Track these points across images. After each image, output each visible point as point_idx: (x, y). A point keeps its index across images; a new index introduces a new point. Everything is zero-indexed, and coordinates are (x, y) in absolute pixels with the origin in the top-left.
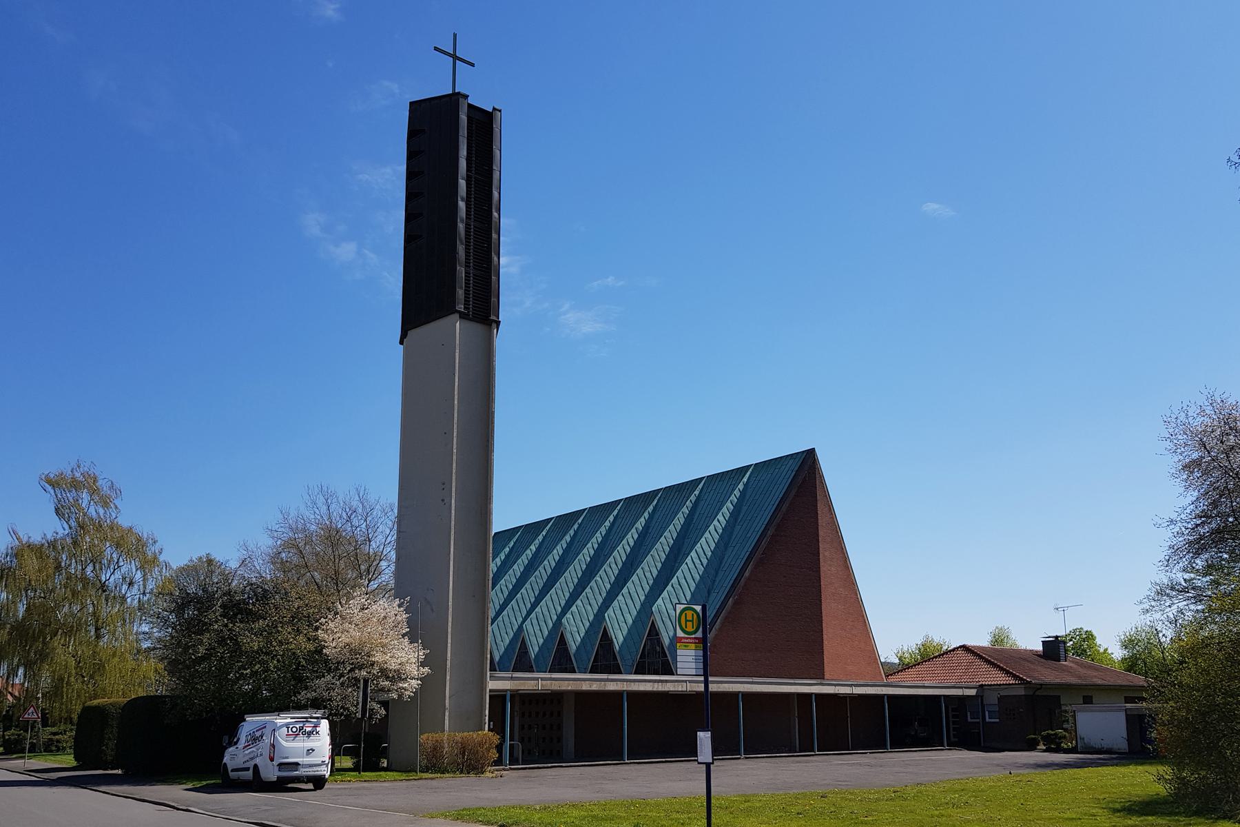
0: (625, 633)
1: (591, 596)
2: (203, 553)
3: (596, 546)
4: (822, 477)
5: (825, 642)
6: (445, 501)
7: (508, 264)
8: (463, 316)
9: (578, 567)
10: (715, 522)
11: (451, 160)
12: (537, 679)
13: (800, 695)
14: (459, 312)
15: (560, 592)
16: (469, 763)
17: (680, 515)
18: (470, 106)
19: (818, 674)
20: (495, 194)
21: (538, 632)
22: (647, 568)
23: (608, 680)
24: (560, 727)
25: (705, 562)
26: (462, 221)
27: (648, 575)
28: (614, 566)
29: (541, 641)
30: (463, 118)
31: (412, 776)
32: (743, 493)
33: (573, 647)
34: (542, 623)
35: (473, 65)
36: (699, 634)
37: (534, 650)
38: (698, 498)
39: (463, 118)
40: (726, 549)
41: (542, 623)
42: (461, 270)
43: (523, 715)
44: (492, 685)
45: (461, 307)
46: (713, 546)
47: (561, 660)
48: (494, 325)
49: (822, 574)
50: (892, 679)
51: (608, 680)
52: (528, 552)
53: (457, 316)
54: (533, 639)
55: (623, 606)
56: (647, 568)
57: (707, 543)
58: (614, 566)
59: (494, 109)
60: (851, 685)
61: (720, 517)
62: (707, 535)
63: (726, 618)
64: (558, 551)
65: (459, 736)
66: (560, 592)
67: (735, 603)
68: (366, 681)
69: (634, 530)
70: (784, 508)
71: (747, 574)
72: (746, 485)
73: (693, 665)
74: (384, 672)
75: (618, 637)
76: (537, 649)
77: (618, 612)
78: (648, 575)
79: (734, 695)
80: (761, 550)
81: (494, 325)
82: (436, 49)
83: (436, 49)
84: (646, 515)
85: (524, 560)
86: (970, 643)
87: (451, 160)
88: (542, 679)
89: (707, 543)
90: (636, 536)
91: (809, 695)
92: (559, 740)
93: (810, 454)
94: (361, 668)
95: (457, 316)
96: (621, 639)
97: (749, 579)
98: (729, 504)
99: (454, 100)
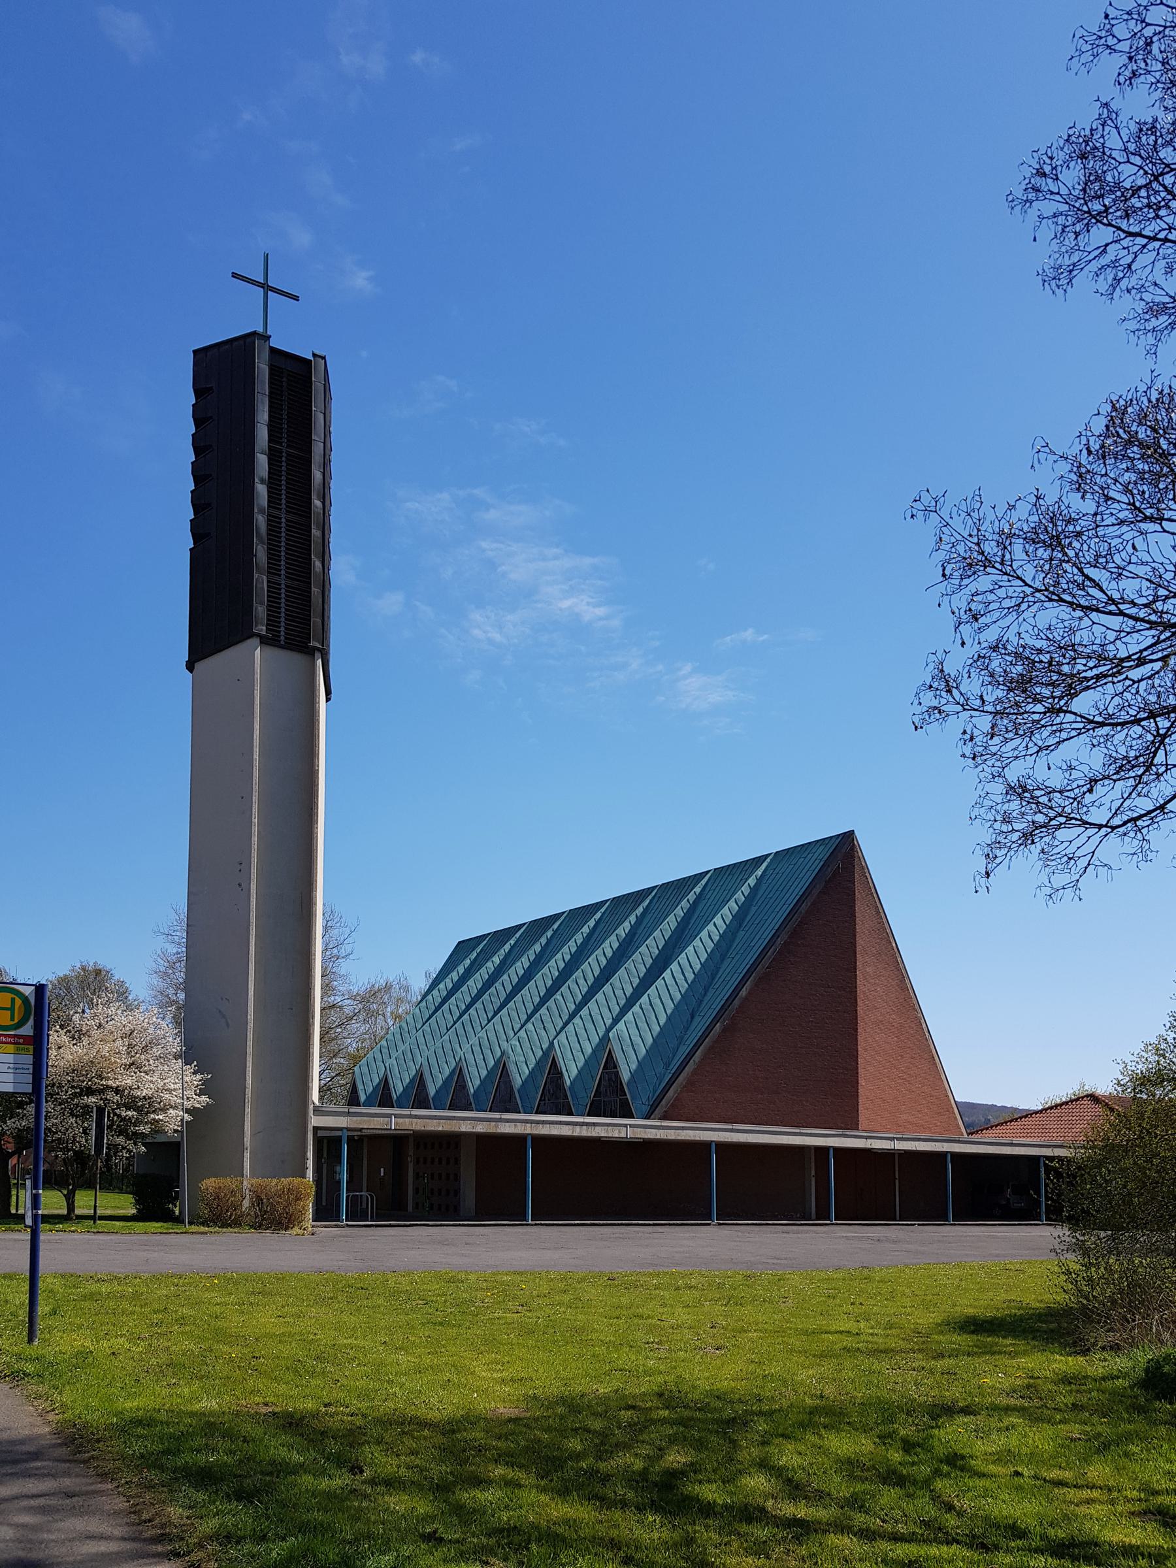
0: (581, 1064)
1: (546, 1018)
2: (109, 967)
3: (567, 957)
4: (865, 869)
5: (862, 1083)
6: (243, 887)
7: (345, 570)
8: (265, 641)
9: (541, 984)
10: (711, 927)
11: (258, 435)
12: (389, 1116)
13: (819, 1149)
14: (261, 637)
15: (513, 1014)
16: (272, 1217)
17: (671, 918)
18: (273, 351)
19: (848, 1121)
20: (317, 475)
21: (481, 1063)
22: (618, 984)
23: (501, 1120)
24: (457, 1177)
25: (690, 977)
26: (262, 511)
27: (619, 992)
28: (581, 982)
29: (484, 1073)
30: (262, 368)
31: (180, 1228)
32: (754, 890)
33: (517, 1082)
34: (487, 1052)
35: (296, 298)
36: (28, 1030)
37: (473, 1084)
38: (699, 897)
39: (262, 368)
40: (723, 960)
41: (487, 1052)
42: (261, 581)
43: (418, 1162)
44: (315, 1121)
45: (262, 629)
46: (704, 957)
47: (554, 1096)
48: (318, 654)
49: (860, 996)
50: (975, 1138)
51: (501, 1120)
52: (489, 964)
53: (256, 641)
54: (473, 1070)
55: (581, 1032)
56: (618, 984)
57: (695, 954)
58: (581, 982)
59: (314, 355)
60: (892, 1139)
61: (718, 920)
62: (697, 942)
63: (711, 1049)
64: (524, 962)
65: (254, 1181)
66: (513, 1014)
67: (724, 1030)
68: (100, 1110)
69: (613, 937)
70: (804, 907)
71: (744, 992)
72: (759, 880)
73: (11, 1078)
74: (132, 1103)
75: (571, 1070)
76: (478, 1082)
77: (573, 1039)
78: (619, 992)
79: (706, 1145)
80: (766, 962)
81: (318, 654)
82: (235, 275)
83: (235, 275)
84: (633, 919)
85: (483, 974)
86: (1089, 1088)
87: (258, 435)
88: (396, 1116)
89: (695, 954)
90: (616, 945)
91: (826, 1149)
92: (457, 1192)
93: (849, 836)
94: (90, 1092)
95: (256, 641)
96: (574, 1072)
97: (746, 998)
98: (732, 903)
99: (245, 345)
